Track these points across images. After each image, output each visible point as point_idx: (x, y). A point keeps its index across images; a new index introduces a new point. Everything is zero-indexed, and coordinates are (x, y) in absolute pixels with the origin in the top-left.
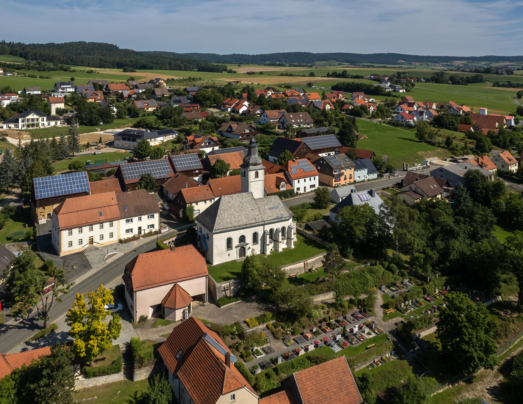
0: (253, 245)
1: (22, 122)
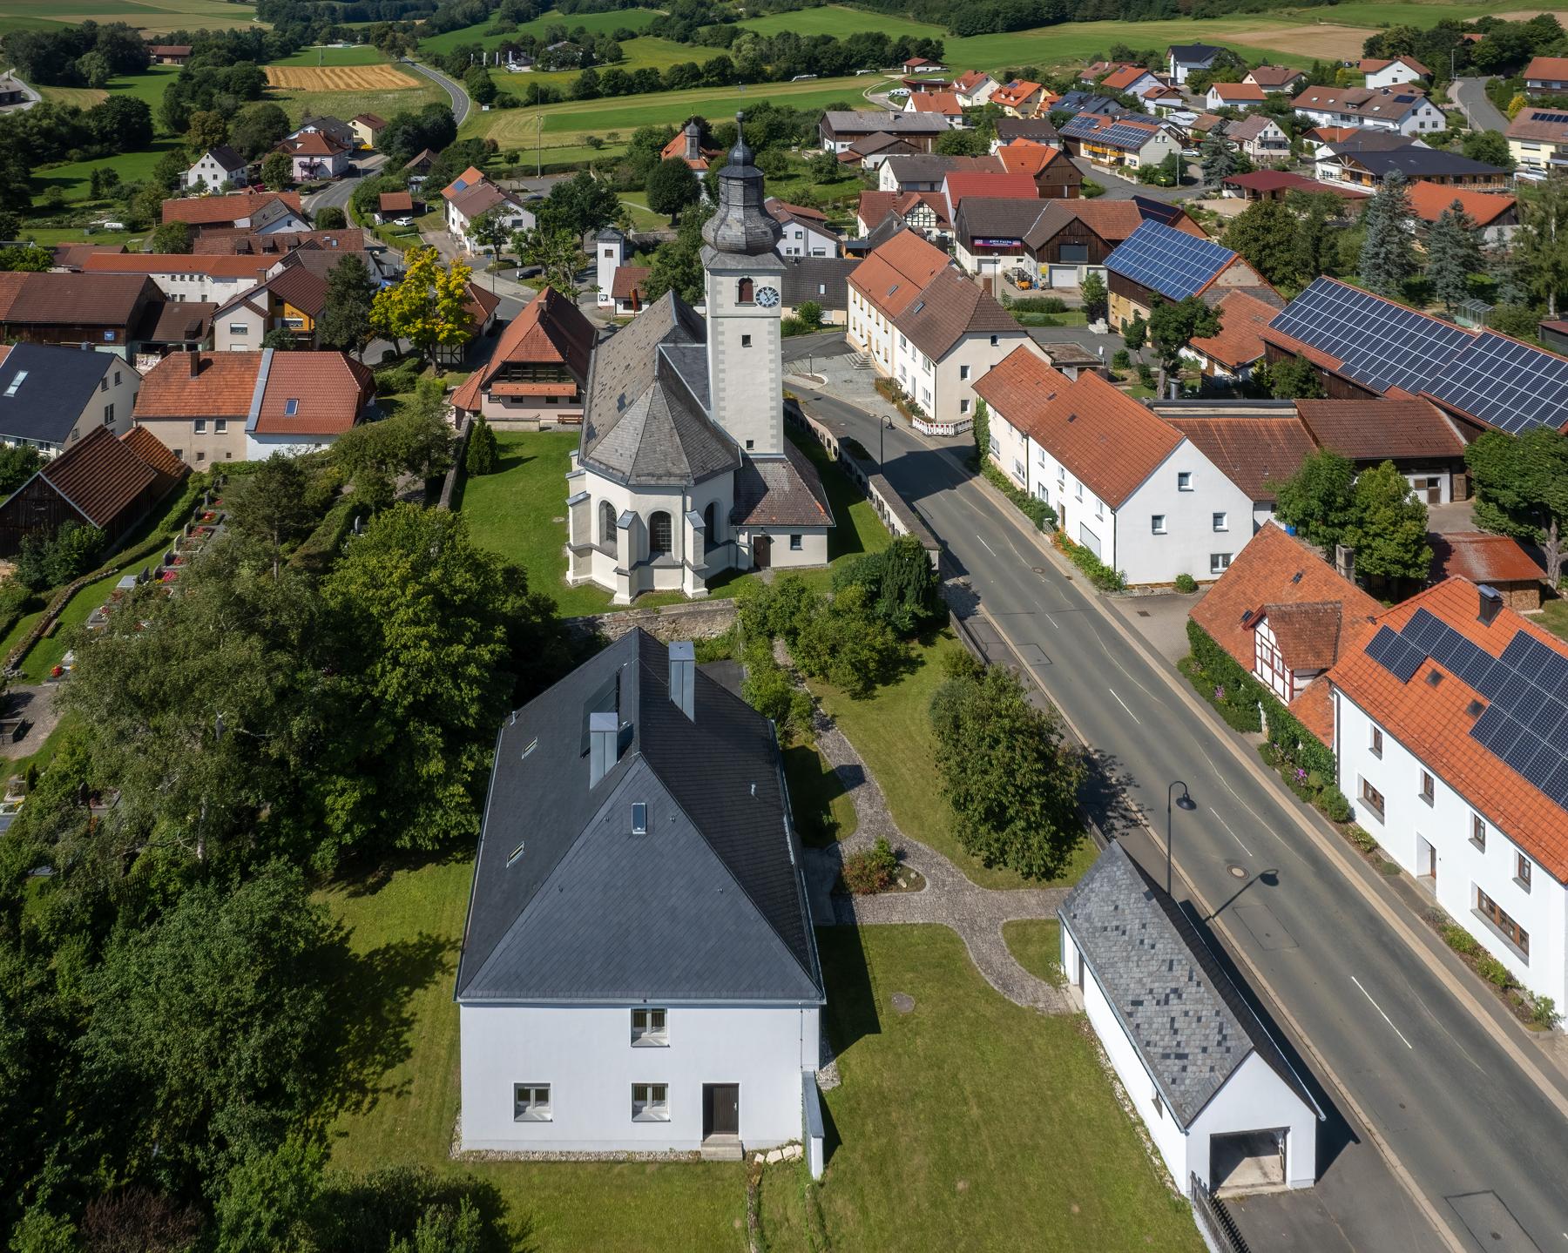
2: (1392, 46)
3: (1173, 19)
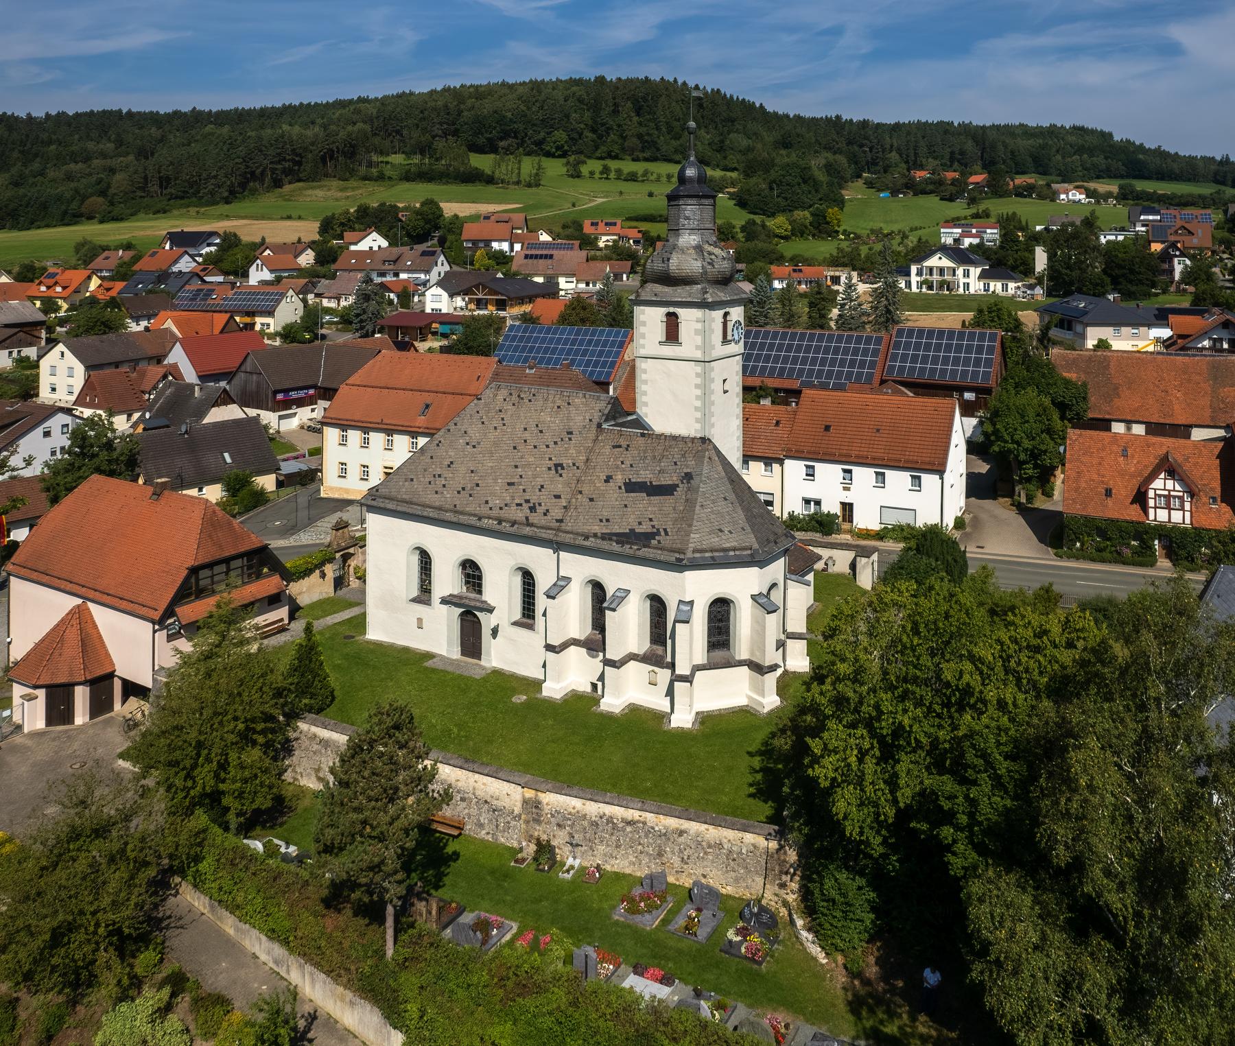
0: (515, 624)
1: (917, 275)
2: (342, 224)
3: (75, 223)
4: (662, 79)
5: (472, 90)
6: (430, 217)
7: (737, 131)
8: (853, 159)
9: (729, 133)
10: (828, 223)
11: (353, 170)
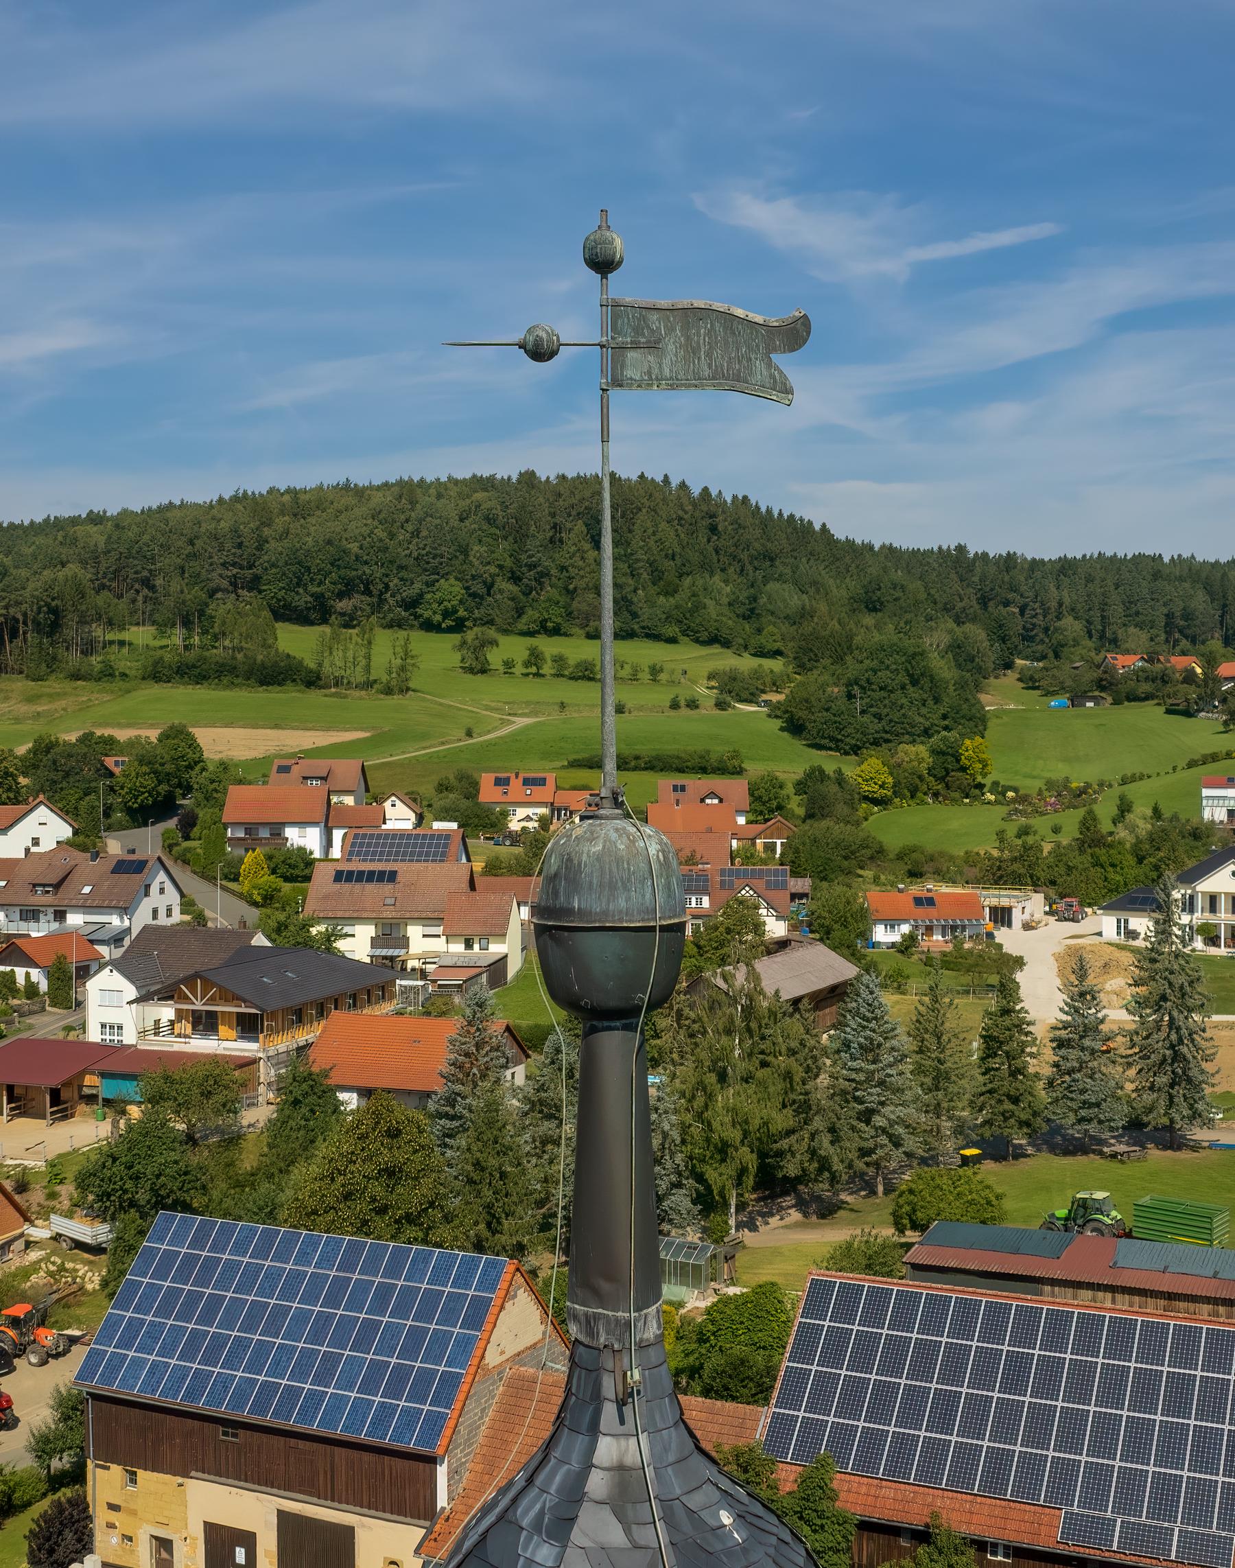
4: (642, 476)
5: (287, 498)
6: (169, 768)
7: (781, 578)
8: (999, 634)
9: (766, 580)
10: (964, 769)
11: (54, 658)
